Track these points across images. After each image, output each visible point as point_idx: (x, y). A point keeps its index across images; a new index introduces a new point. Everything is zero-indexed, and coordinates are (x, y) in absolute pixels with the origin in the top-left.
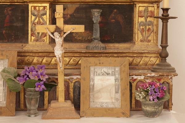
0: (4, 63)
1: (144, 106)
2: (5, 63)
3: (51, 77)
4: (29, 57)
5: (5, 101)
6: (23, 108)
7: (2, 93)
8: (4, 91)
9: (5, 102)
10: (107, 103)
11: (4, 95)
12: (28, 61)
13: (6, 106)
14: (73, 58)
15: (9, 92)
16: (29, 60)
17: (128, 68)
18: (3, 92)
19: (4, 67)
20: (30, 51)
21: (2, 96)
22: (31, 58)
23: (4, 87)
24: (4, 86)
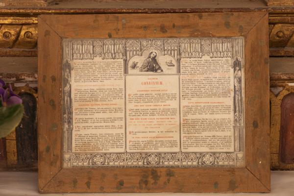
0: (232, 47)
1: (148, 163)
2: (236, 48)
3: (95, 88)
4: (280, 25)
5: (240, 151)
6: (277, 164)
7: (232, 130)
8: (238, 125)
9: (240, 155)
10: (105, 154)
11: (237, 134)
12: (278, 36)
13: (244, 166)
14: (24, 27)
15: (252, 128)
16: (281, 34)
17: (40, 53)
18: (234, 127)
19: (233, 57)
20: (109, 11)
21: (233, 139)
22: (286, 28)
23: (237, 113)
24: (235, 111)
